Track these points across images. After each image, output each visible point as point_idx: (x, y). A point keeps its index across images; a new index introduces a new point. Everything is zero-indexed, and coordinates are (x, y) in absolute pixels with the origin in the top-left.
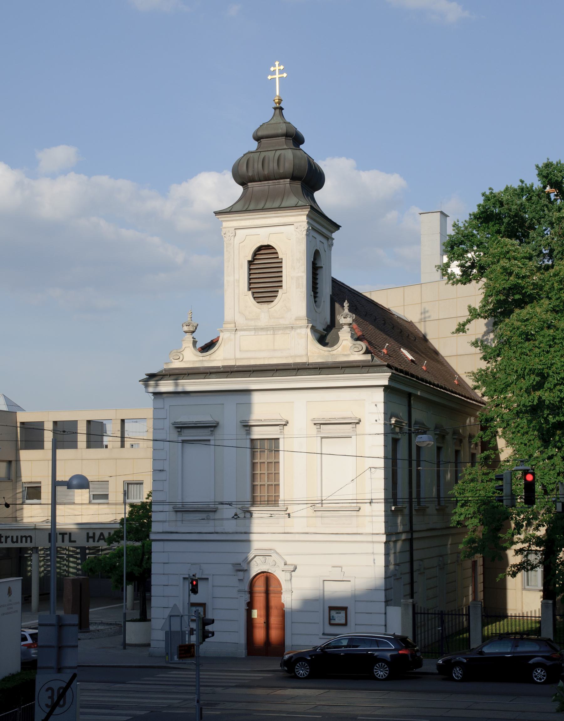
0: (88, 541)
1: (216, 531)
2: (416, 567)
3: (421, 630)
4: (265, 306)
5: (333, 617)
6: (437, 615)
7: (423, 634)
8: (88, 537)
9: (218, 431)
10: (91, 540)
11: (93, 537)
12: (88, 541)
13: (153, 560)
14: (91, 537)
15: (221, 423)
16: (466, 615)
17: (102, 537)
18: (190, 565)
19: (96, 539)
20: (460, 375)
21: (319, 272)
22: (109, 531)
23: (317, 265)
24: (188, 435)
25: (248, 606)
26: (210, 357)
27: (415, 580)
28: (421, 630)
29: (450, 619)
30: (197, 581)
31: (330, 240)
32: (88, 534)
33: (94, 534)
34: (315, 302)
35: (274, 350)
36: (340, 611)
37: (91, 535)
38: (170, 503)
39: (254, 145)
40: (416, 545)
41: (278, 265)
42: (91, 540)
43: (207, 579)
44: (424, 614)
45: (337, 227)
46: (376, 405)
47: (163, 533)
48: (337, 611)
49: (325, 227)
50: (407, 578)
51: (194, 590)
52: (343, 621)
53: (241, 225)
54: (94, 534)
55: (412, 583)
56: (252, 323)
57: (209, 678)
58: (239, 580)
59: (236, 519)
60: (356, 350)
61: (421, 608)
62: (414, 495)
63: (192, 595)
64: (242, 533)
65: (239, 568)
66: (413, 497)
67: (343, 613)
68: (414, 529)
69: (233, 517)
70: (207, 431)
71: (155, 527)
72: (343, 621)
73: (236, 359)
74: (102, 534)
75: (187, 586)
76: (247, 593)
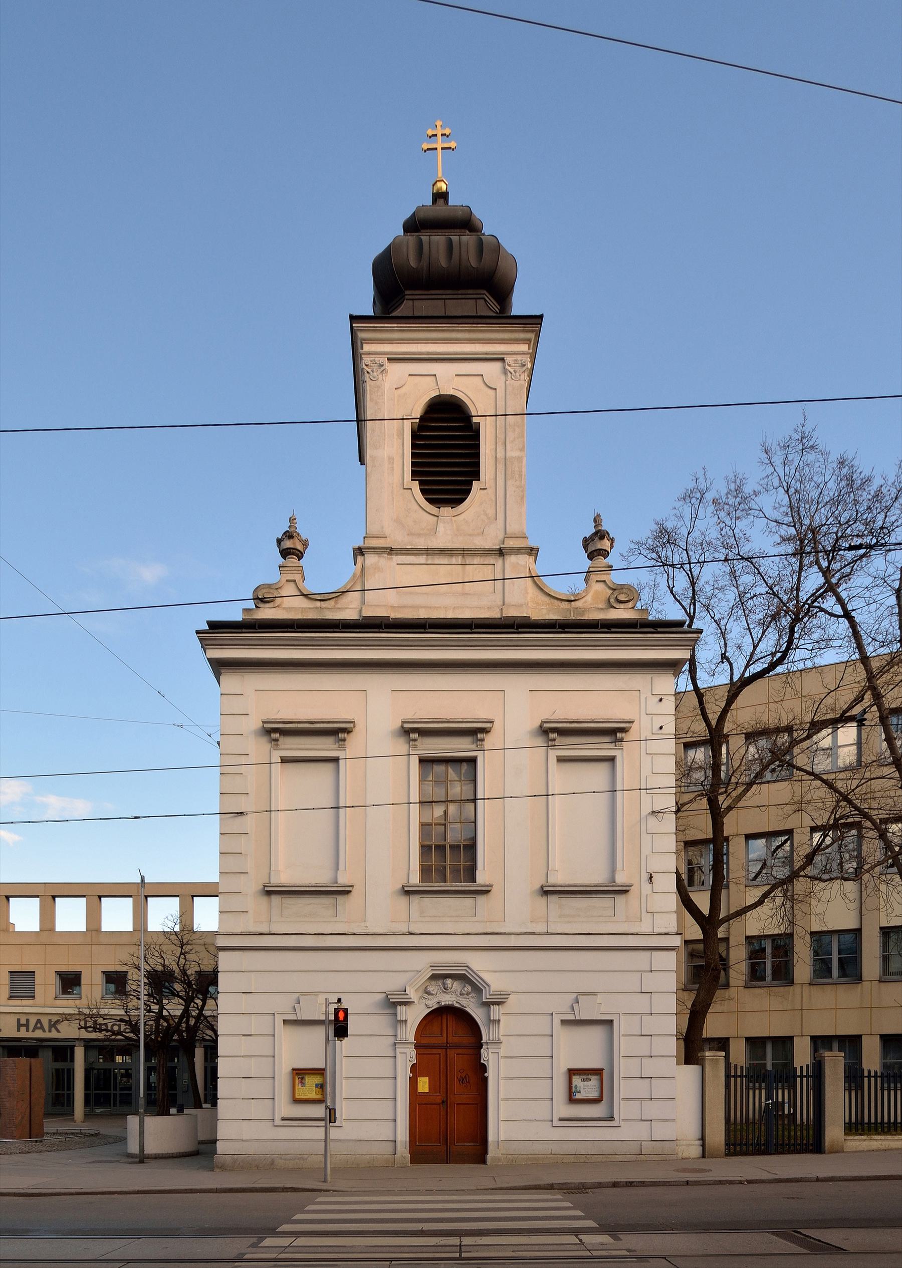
0: (19, 1030)
4: (446, 511)
8: (19, 1025)
10: (23, 1029)
11: (27, 1025)
12: (19, 1030)
14: (23, 1025)
17: (39, 1025)
19: (31, 1027)
22: (50, 1017)
26: (336, 603)
32: (19, 1020)
33: (28, 1020)
36: (590, 1077)
37: (23, 1022)
41: (473, 434)
42: (23, 1029)
48: (585, 1077)
52: (594, 1094)
54: (28, 1020)
57: (458, 1210)
61: (736, 1066)
67: (594, 1081)
70: (328, 741)
74: (39, 1021)
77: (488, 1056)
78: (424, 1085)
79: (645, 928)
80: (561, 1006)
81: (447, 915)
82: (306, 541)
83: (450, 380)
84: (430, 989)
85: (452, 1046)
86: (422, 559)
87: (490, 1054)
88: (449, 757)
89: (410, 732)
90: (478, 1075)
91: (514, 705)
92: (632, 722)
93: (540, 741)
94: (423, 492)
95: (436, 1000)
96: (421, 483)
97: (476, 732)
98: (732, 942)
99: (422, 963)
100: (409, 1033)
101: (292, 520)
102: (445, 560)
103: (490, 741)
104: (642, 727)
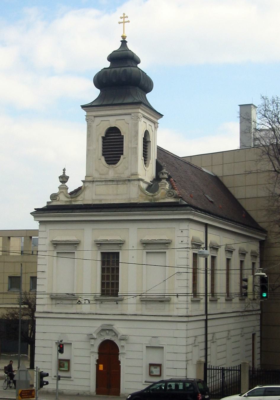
1: (187, 318)
2: (209, 337)
3: (214, 379)
5: (152, 371)
6: (237, 371)
7: (215, 382)
9: (80, 248)
13: (37, 329)
15: (127, 241)
16: (238, 370)
18: (60, 334)
20: (249, 212)
21: (148, 144)
23: (147, 140)
24: (61, 249)
25: (97, 362)
27: (208, 346)
28: (214, 379)
29: (217, 372)
30: (63, 345)
31: (156, 124)
34: (145, 164)
35: (117, 195)
38: (48, 294)
39: (108, 64)
40: (209, 322)
43: (163, 348)
44: (214, 369)
45: (162, 116)
46: (182, 231)
47: (43, 312)
48: (155, 367)
49: (153, 116)
50: (203, 346)
51: (61, 350)
52: (158, 373)
53: (117, 113)
55: (206, 349)
56: (103, 177)
58: (91, 345)
59: (79, 304)
60: (169, 195)
62: (209, 291)
63: (59, 354)
64: (93, 314)
65: (91, 337)
66: (208, 292)
67: (158, 369)
68: (208, 313)
69: (77, 303)
71: (38, 309)
72: (158, 373)
73: (93, 200)
75: (55, 349)
76: (96, 353)
77: (121, 358)
78: (101, 367)
79: (175, 314)
80: (147, 341)
81: (109, 308)
82: (67, 178)
83: (113, 122)
84: (102, 334)
85: (109, 355)
86: (104, 183)
87: (121, 358)
88: (110, 263)
89: (99, 244)
90: (117, 364)
91: (131, 235)
92: (234, 250)
93: (141, 247)
94: (106, 160)
95: (104, 338)
96: (105, 158)
97: (120, 244)
98: (79, 306)
99: (98, 325)
100: (96, 349)
101: (64, 170)
102: (111, 183)
103: (124, 247)
104: (176, 243)
